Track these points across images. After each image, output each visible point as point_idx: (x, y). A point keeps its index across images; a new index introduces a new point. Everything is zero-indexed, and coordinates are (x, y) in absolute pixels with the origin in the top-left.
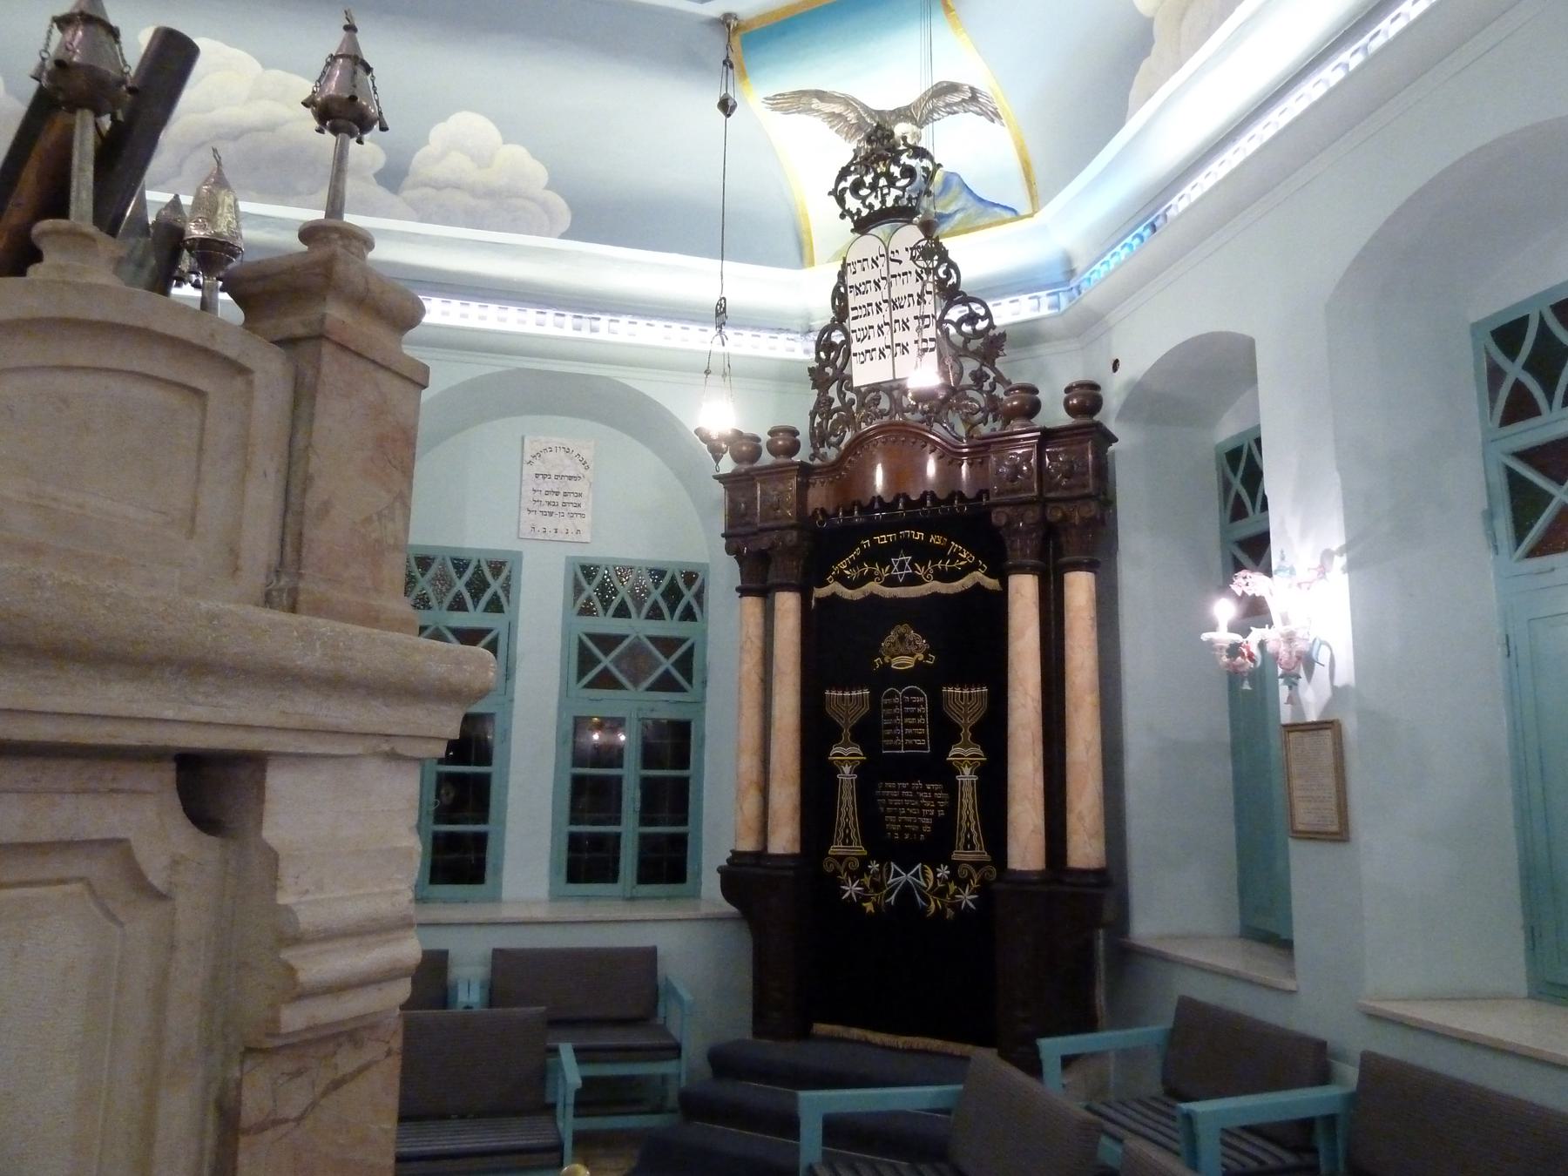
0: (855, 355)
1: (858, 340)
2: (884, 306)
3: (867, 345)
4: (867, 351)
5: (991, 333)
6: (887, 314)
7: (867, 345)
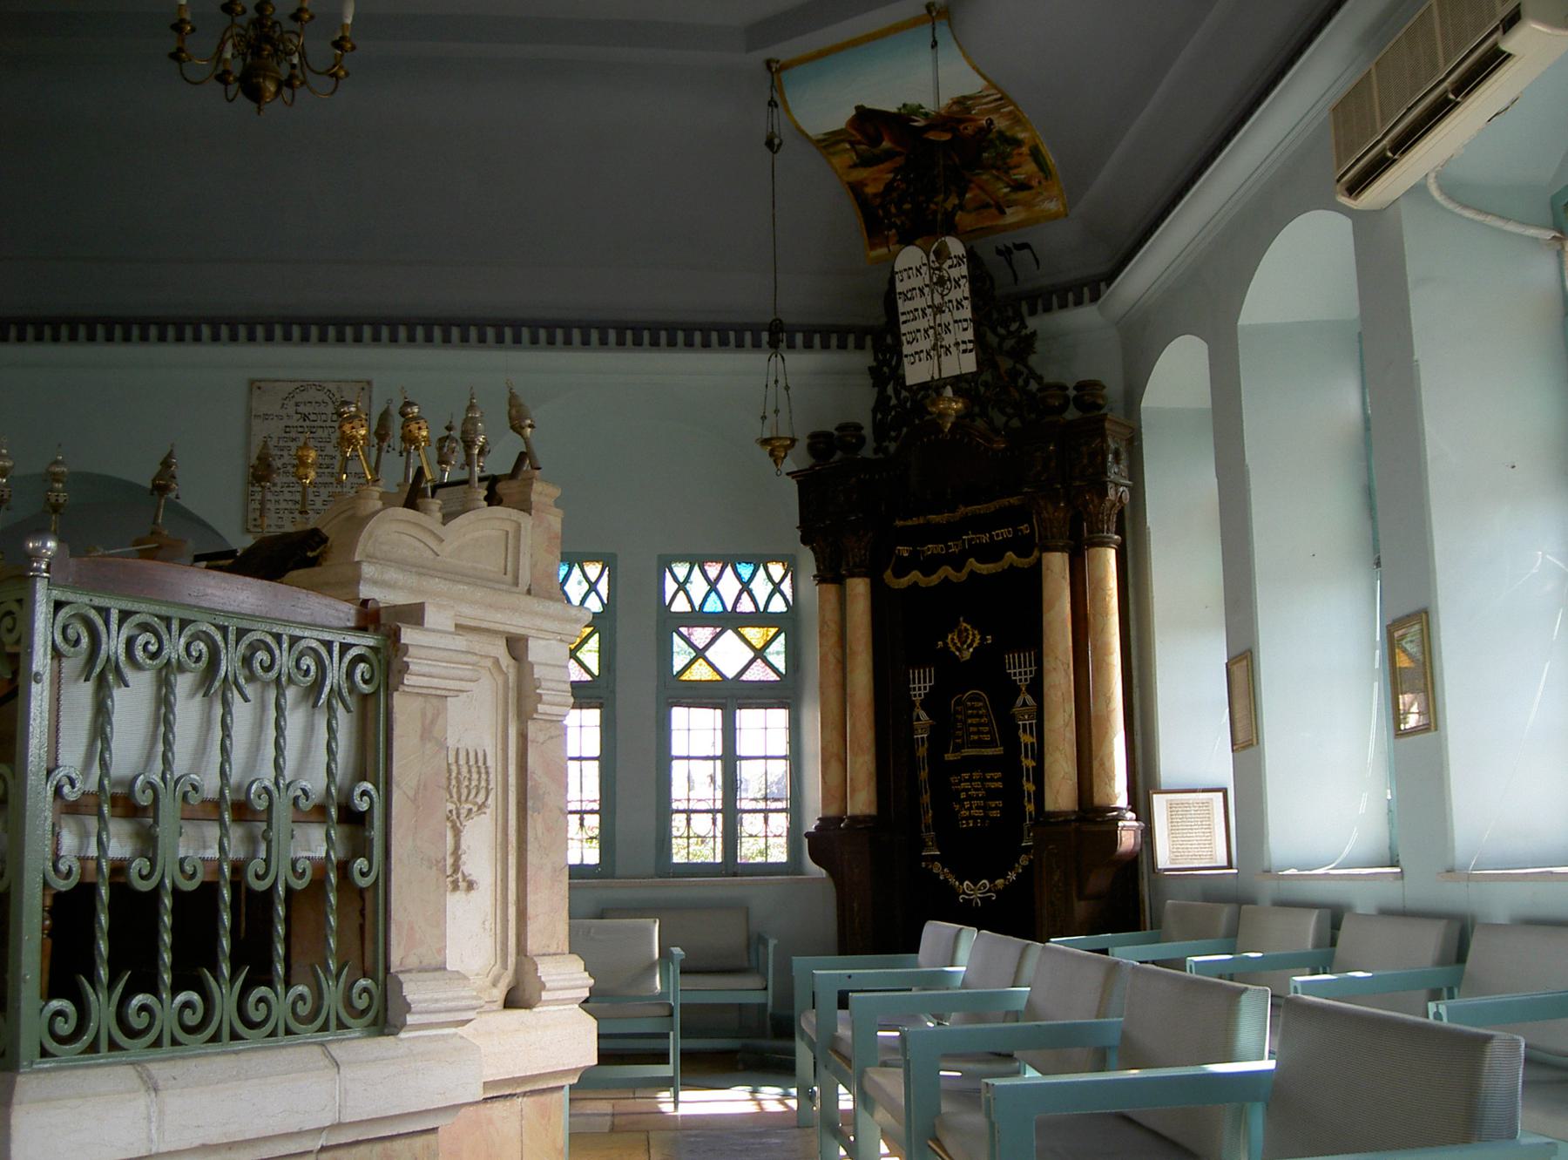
0: (906, 356)
1: (908, 342)
2: (929, 311)
3: (916, 347)
4: (916, 353)
5: (1024, 332)
6: (931, 318)
7: (916, 347)
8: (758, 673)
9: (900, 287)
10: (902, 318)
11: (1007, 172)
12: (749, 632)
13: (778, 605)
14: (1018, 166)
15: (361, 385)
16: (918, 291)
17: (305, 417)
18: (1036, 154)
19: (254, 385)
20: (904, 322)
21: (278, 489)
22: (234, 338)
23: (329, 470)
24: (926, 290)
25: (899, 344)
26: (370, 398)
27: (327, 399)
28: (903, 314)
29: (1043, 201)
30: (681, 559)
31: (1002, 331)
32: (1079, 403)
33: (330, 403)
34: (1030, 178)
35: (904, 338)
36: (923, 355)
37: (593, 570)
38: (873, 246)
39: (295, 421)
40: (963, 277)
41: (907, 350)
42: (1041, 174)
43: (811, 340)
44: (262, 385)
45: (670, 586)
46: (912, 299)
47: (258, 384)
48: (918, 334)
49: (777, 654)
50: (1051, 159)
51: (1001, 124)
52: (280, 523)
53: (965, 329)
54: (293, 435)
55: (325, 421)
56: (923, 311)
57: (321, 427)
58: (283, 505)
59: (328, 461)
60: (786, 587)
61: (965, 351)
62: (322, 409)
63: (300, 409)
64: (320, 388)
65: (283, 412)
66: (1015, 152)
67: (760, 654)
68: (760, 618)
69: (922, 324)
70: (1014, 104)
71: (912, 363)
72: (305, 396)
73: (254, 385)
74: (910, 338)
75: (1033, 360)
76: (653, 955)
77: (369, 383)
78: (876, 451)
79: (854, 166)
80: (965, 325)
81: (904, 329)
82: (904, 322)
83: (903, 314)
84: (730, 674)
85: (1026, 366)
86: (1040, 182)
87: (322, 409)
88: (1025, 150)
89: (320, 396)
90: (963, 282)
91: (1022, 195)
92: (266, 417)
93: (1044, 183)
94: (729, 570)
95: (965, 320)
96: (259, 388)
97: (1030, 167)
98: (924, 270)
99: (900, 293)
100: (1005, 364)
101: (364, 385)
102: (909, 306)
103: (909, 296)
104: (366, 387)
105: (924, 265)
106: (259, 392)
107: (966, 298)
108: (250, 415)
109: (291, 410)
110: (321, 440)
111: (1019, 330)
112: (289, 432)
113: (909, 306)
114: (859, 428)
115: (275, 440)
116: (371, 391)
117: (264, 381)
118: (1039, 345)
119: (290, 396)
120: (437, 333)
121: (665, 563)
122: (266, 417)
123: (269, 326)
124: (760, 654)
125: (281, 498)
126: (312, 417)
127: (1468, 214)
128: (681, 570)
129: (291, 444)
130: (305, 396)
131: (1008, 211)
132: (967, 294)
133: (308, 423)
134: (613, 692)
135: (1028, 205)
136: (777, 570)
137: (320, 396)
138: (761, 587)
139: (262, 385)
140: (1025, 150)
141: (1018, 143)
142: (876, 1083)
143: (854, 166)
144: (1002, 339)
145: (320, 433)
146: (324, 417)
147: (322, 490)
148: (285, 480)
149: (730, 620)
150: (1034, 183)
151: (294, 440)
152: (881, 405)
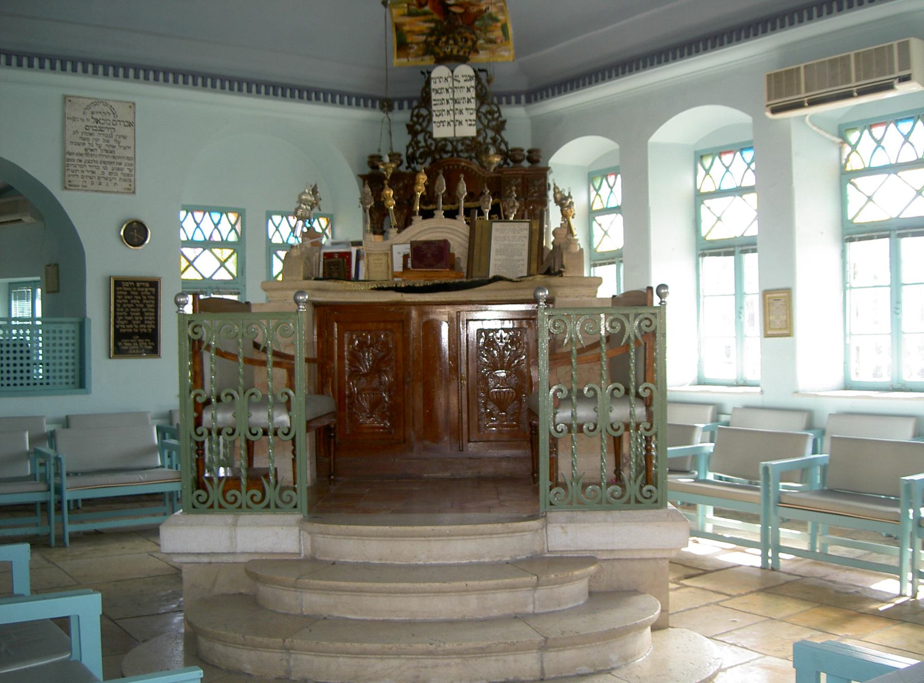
0: (435, 122)
2: (451, 101)
4: (441, 122)
7: (441, 119)
8: (223, 275)
9: (433, 86)
10: (433, 103)
11: (485, 33)
12: (216, 251)
13: (233, 238)
14: (493, 31)
15: (129, 104)
16: (445, 90)
17: (97, 121)
18: (504, 28)
19: (66, 99)
20: (435, 105)
21: (83, 164)
22: (95, 73)
23: (113, 154)
24: (450, 90)
25: (430, 114)
26: (135, 113)
27: (110, 112)
28: (434, 100)
29: (502, 51)
30: (277, 213)
31: (489, 117)
32: (530, 159)
33: (112, 114)
34: (497, 38)
35: (434, 114)
36: (446, 124)
37: (233, 217)
38: (398, 57)
39: (91, 123)
40: (472, 87)
41: (435, 119)
42: (503, 38)
43: (359, 101)
44: (71, 99)
45: (271, 229)
46: (441, 93)
47: (69, 98)
48: (444, 113)
49: (232, 265)
50: (511, 32)
51: (493, 10)
52: (84, 185)
53: (471, 114)
54: (91, 131)
55: (109, 124)
56: (447, 101)
57: (107, 128)
58: (86, 174)
59: (111, 149)
60: (238, 227)
61: (470, 125)
62: (107, 117)
63: (94, 116)
64: (106, 104)
65: (84, 117)
66: (493, 24)
67: (223, 264)
68: (224, 244)
69: (446, 107)
70: (505, 4)
71: (439, 127)
72: (97, 108)
73: (66, 99)
74: (438, 113)
75: (503, 133)
76: (26, 448)
77: (134, 104)
78: (407, 168)
79: (404, 15)
80: (472, 111)
81: (434, 108)
82: (435, 105)
83: (434, 100)
84: (207, 276)
85: (501, 137)
86: (502, 42)
87: (107, 117)
88: (499, 24)
89: (107, 109)
90: (472, 89)
91: (491, 46)
92: (74, 119)
93: (504, 42)
94: (190, 214)
95: (472, 109)
96: (70, 101)
97: (498, 33)
98: (449, 79)
99: (433, 89)
100: (490, 134)
101: (131, 105)
102: (438, 97)
103: (439, 91)
104: (132, 106)
105: (450, 77)
106: (69, 103)
107: (473, 98)
108: (64, 117)
109: (89, 116)
110: (107, 136)
111: (498, 117)
112: (88, 130)
113: (438, 97)
114: (400, 155)
115: (80, 133)
116: (135, 109)
117: (73, 96)
118: (507, 126)
119: (88, 107)
120: (131, 72)
121: (269, 216)
122: (74, 119)
123: (95, 65)
124: (223, 264)
125: (84, 169)
126: (101, 121)
127: (815, 128)
128: (277, 219)
129: (89, 137)
130: (97, 108)
131: (481, 52)
132: (474, 96)
133: (99, 125)
134: (244, 286)
135: (493, 52)
136: (233, 217)
137: (107, 109)
138: (225, 227)
139: (71, 99)
140: (499, 24)
141: (496, 20)
142: (518, 447)
143: (404, 15)
144: (489, 121)
145: (106, 131)
146: (108, 122)
147: (108, 166)
148: (87, 158)
149: (208, 244)
150: (499, 41)
151: (91, 134)
152: (414, 143)
